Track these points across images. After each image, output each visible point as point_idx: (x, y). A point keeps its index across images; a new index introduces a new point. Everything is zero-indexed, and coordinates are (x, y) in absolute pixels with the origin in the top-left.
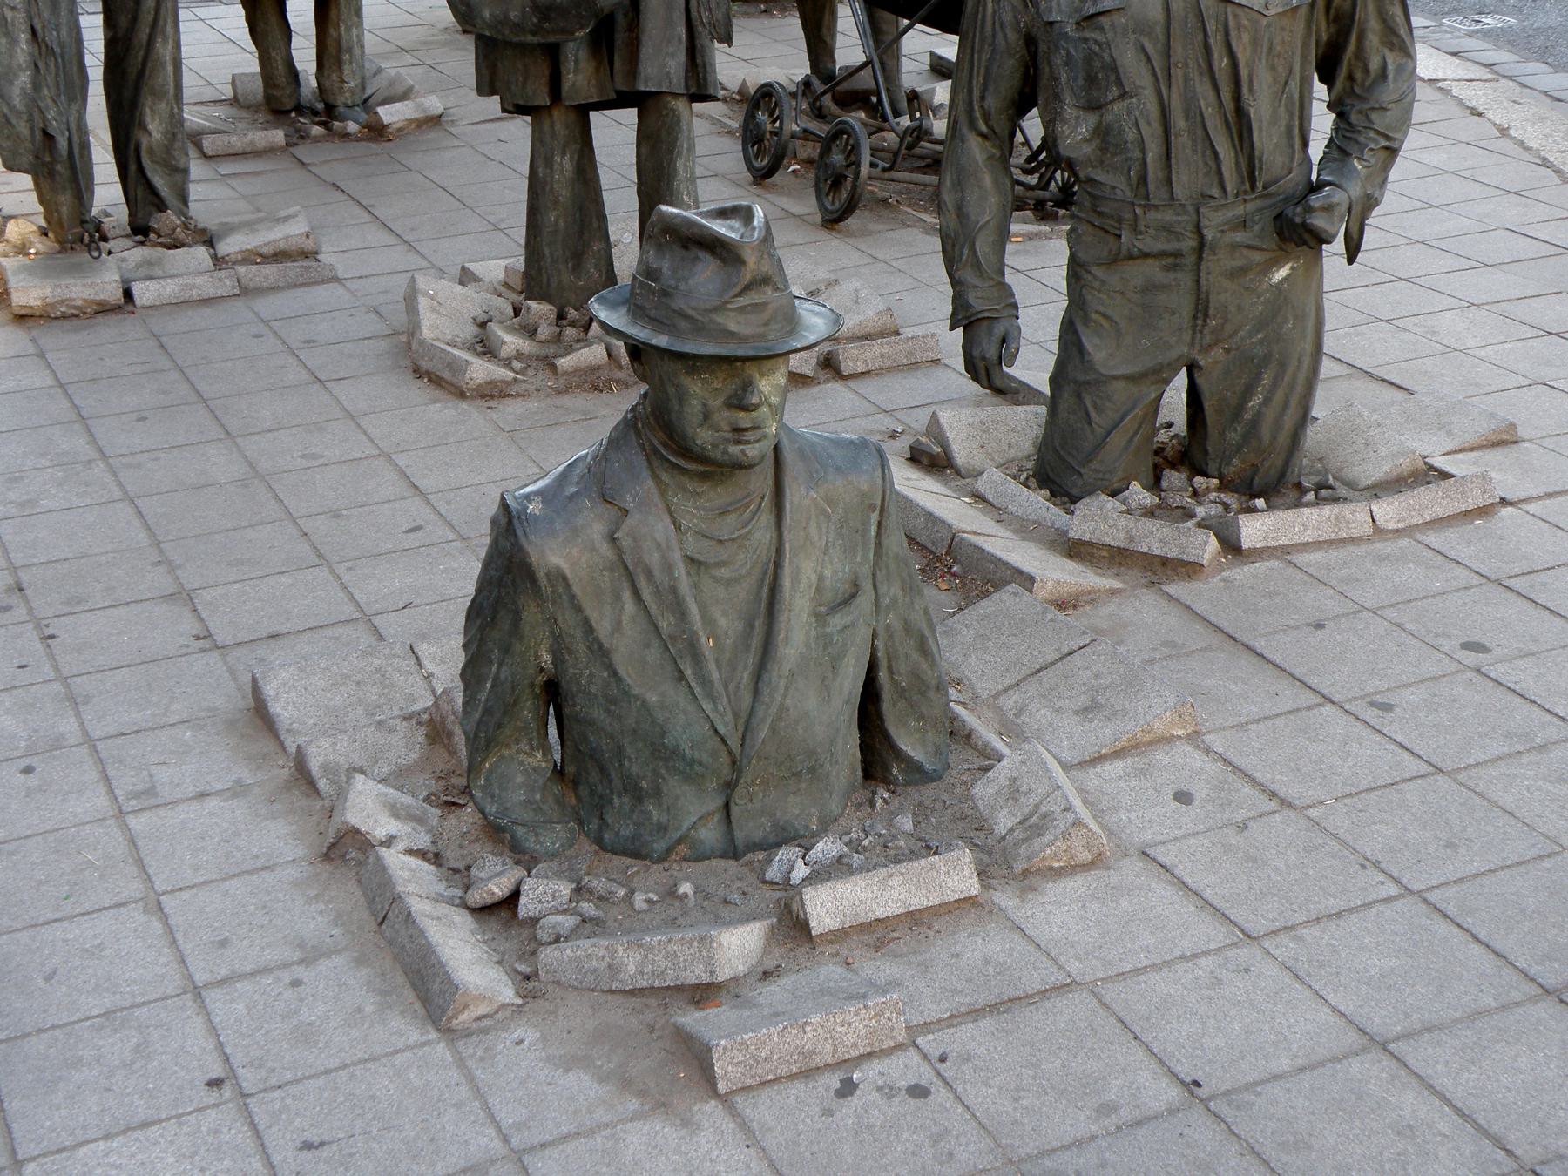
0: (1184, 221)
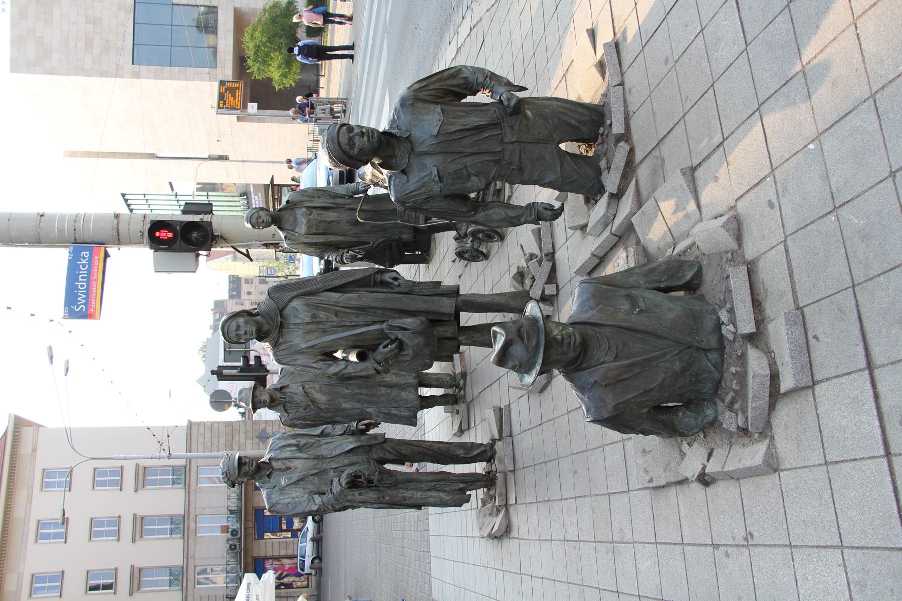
0: (510, 147)
